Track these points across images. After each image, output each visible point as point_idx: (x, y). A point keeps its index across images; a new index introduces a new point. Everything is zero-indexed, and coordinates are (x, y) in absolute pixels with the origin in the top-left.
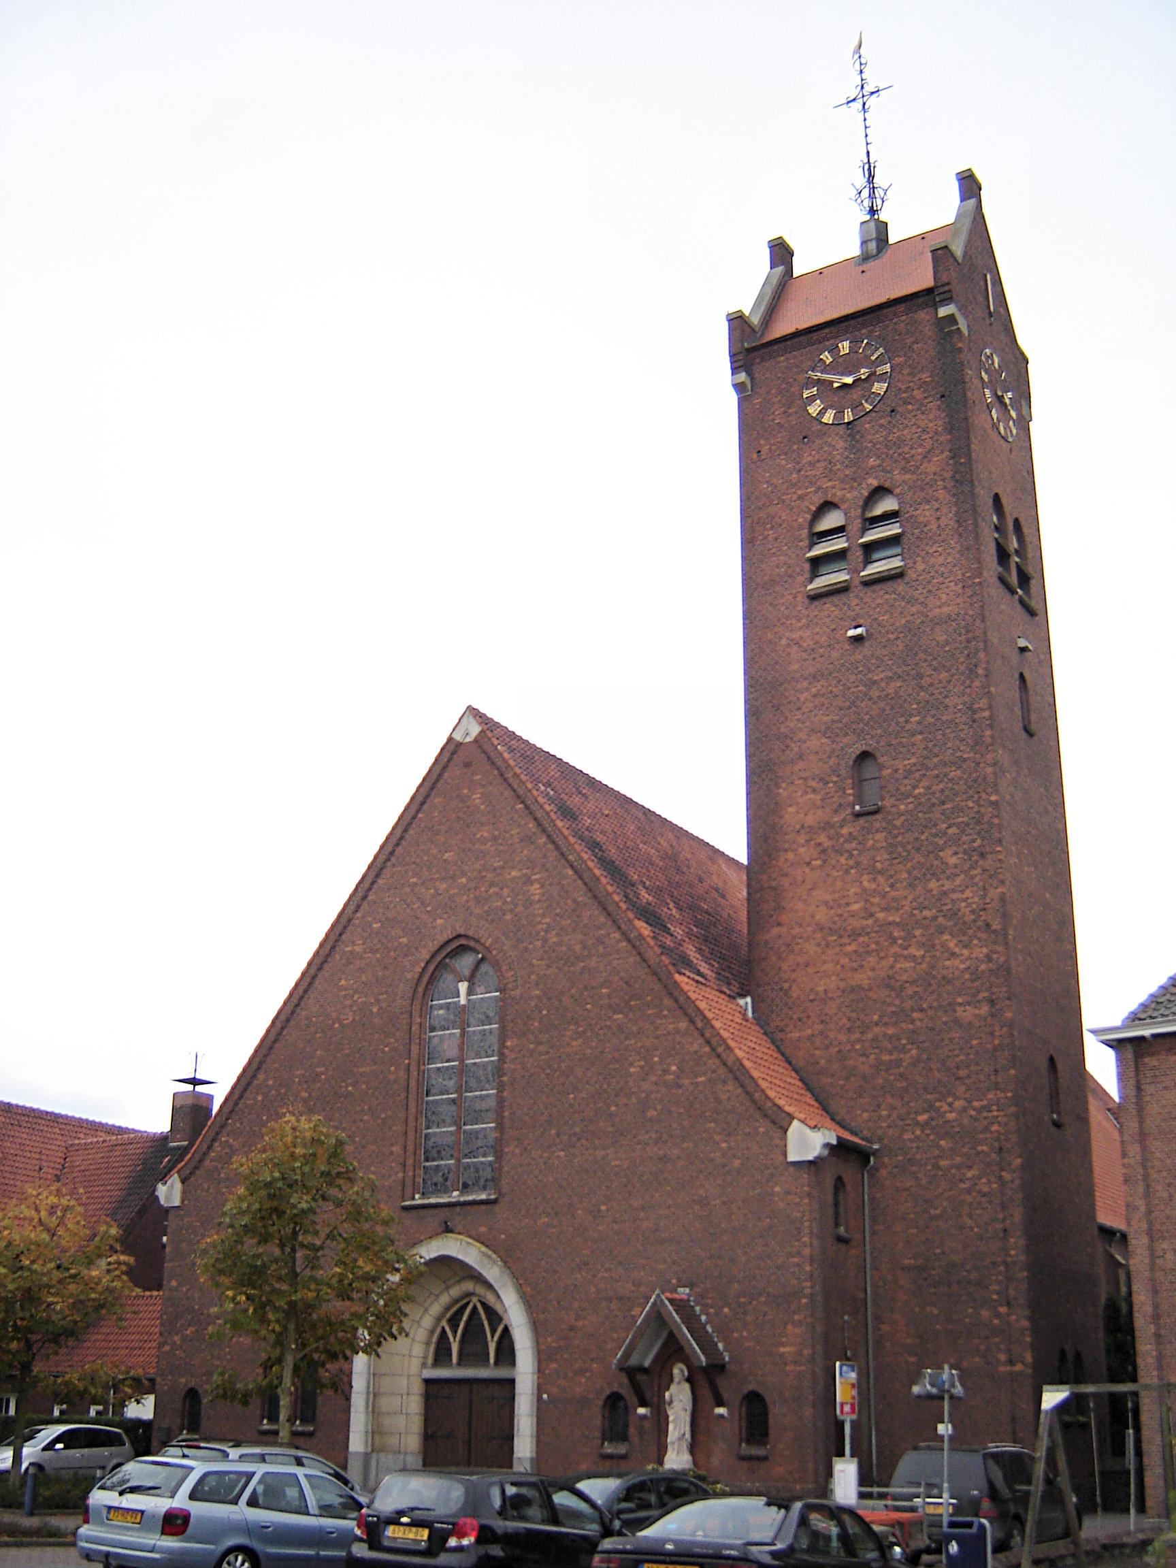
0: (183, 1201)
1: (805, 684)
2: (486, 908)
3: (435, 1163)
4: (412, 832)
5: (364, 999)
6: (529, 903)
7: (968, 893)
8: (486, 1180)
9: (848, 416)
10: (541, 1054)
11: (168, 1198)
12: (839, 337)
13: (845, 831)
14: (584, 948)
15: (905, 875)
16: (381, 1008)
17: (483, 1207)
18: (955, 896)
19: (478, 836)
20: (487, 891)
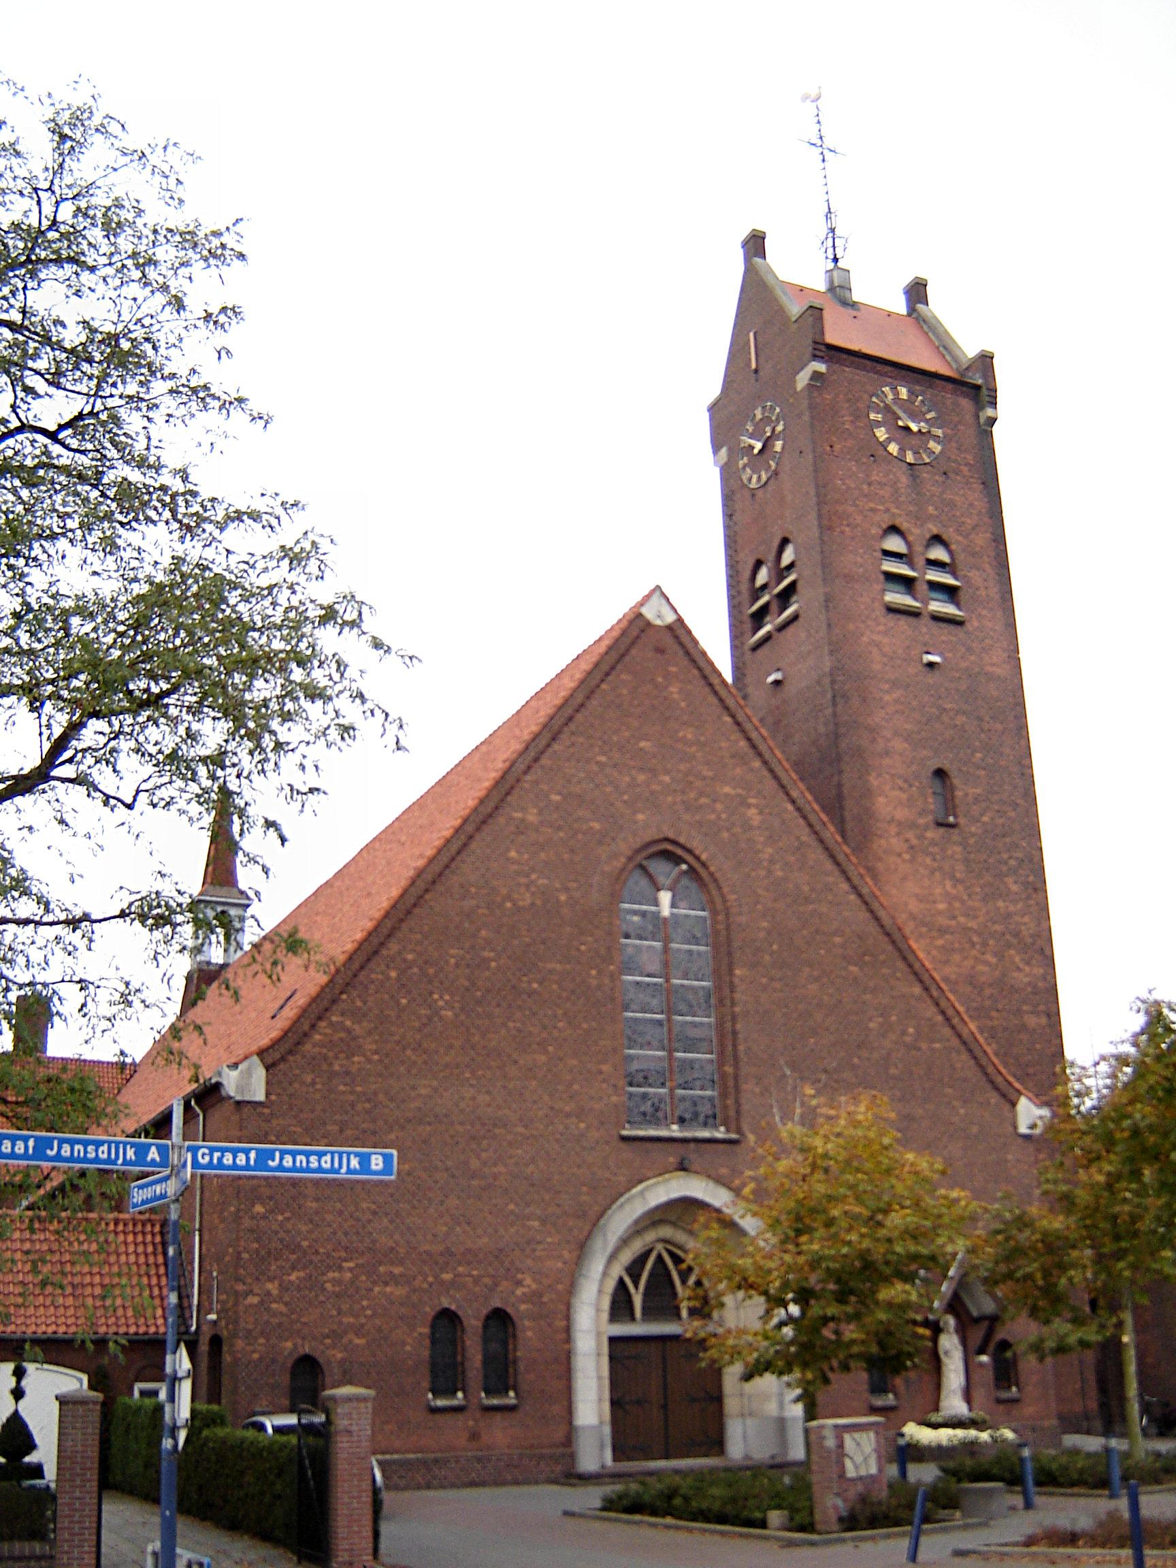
0: (268, 1094)
1: (887, 686)
2: (697, 818)
3: (642, 1090)
4: (594, 702)
5: (546, 881)
6: (746, 826)
7: (1026, 919)
8: (707, 1117)
9: (910, 458)
10: (775, 990)
11: (240, 1088)
12: (907, 382)
13: (929, 834)
14: (813, 890)
15: (978, 890)
16: (571, 898)
17: (722, 1146)
18: (1017, 918)
19: (681, 734)
20: (696, 800)
